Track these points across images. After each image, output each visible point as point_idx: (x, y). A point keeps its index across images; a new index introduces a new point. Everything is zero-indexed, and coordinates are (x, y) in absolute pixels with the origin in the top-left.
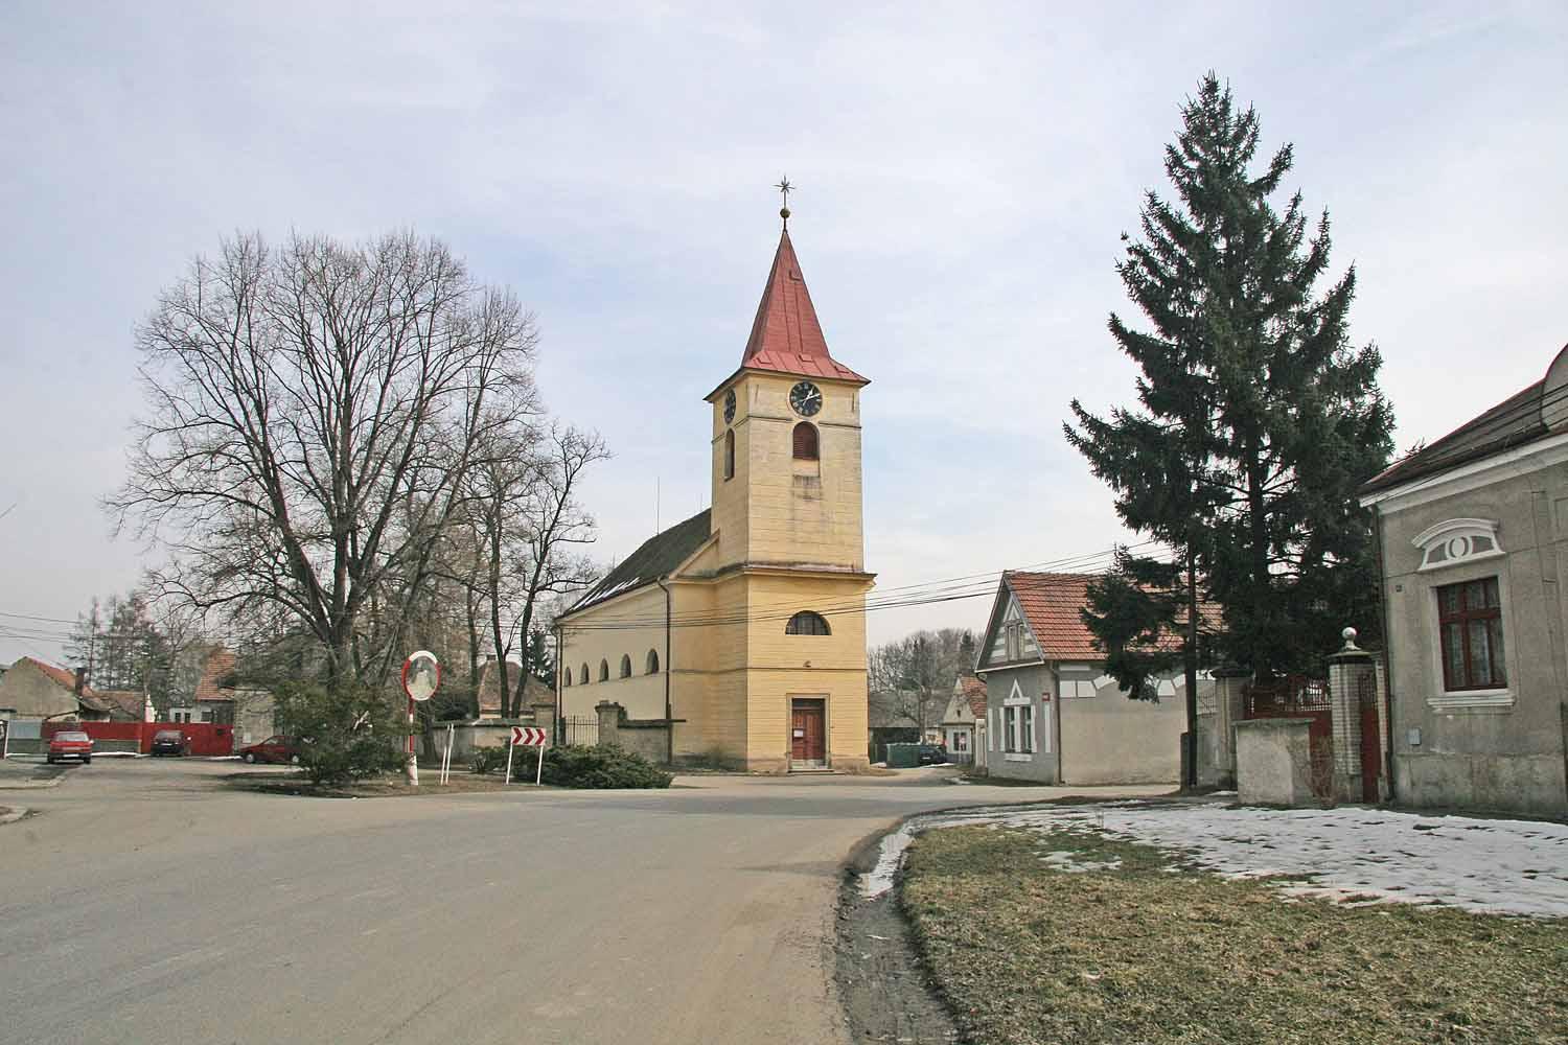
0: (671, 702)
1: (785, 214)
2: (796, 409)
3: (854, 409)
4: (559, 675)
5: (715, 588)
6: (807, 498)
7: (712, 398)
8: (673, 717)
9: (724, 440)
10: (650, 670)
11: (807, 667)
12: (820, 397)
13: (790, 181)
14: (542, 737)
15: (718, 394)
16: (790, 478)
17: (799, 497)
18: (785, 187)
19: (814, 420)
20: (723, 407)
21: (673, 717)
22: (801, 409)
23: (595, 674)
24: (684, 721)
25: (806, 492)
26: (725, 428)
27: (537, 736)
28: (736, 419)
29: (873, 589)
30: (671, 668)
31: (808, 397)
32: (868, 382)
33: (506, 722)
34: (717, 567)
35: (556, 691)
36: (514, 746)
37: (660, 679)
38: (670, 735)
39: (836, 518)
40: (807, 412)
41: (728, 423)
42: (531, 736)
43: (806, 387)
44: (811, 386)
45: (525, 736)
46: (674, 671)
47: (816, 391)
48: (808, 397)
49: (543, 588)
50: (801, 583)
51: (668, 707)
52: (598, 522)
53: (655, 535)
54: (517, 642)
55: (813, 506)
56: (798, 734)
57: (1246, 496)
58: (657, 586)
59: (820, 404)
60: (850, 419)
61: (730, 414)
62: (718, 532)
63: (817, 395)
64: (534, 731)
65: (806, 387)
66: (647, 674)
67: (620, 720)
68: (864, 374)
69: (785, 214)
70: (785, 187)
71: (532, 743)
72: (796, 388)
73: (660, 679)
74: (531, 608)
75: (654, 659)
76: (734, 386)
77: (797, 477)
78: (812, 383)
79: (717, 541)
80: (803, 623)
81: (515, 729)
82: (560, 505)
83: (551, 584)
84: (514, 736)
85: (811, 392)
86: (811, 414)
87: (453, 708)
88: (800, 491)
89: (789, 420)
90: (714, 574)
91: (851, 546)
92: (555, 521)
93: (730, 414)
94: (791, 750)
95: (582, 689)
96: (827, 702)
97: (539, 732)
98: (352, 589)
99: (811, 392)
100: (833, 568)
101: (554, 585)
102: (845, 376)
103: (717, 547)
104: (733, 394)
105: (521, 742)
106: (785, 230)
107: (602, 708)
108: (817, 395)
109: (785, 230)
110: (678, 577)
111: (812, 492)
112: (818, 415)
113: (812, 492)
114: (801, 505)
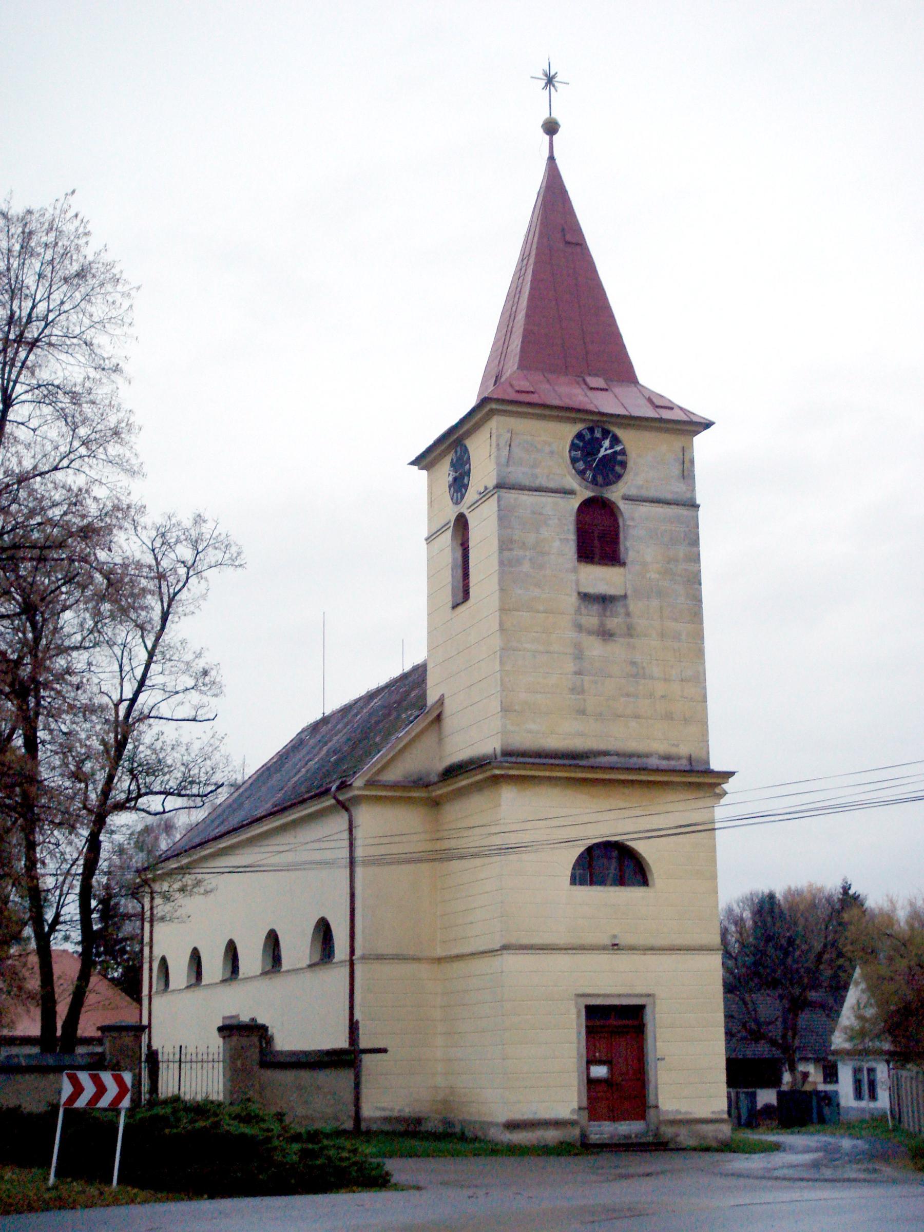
0: (358, 1016)
1: (551, 128)
2: (581, 473)
3: (686, 472)
4: (146, 966)
5: (435, 804)
6: (606, 634)
7: (424, 463)
8: (364, 1044)
9: (449, 534)
10: (317, 958)
11: (615, 946)
12: (623, 452)
13: (558, 69)
14: (123, 1089)
15: (479, 416)
16: (573, 599)
17: (590, 633)
18: (550, 80)
19: (615, 494)
20: (445, 471)
21: (364, 1044)
22: (589, 474)
23: (213, 967)
24: (384, 1051)
25: (602, 625)
26: (450, 513)
27: (112, 1089)
28: (471, 495)
29: (723, 801)
30: (358, 953)
31: (602, 453)
32: (708, 425)
33: (50, 1061)
34: (441, 766)
35: (141, 1005)
36: (66, 1111)
37: (337, 976)
38: (357, 1077)
39: (656, 671)
40: (600, 479)
41: (457, 503)
42: (101, 1090)
43: (598, 434)
44: (606, 433)
45: (90, 1089)
46: (363, 958)
47: (616, 440)
48: (602, 453)
49: (121, 807)
50: (626, 790)
51: (353, 1027)
52: (224, 675)
53: (319, 716)
54: (72, 910)
55: (617, 650)
56: (600, 1071)
57: (552, 87)
58: (333, 801)
59: (623, 464)
60: (676, 489)
61: (459, 485)
62: (441, 702)
63: (618, 448)
64: (107, 1077)
65: (598, 434)
66: (310, 966)
67: (262, 1052)
68: (699, 409)
69: (551, 128)
70: (550, 80)
71: (104, 1102)
72: (579, 436)
73: (337, 976)
74: (98, 844)
75: (324, 930)
76: (468, 434)
77: (586, 597)
78: (608, 427)
79: (439, 718)
80: (599, 863)
81: (68, 1075)
82: (151, 654)
83: (136, 799)
84: (67, 1089)
85: (607, 443)
86: (608, 483)
87: (66, 529)
88: (591, 619)
89: (571, 492)
90: (433, 778)
91: (686, 721)
92: (142, 683)
93: (459, 485)
94: (585, 1103)
95: (198, 995)
96: (648, 1011)
97: (119, 1081)
98: (415, 797)
99: (607, 443)
100: (654, 762)
101: (140, 800)
102: (666, 414)
103: (440, 728)
104: (466, 450)
105: (81, 1103)
106: (551, 158)
107: (229, 1030)
108: (618, 448)
109: (551, 158)
110: (370, 784)
111: (613, 623)
112: (621, 484)
113: (613, 623)
114: (595, 648)
